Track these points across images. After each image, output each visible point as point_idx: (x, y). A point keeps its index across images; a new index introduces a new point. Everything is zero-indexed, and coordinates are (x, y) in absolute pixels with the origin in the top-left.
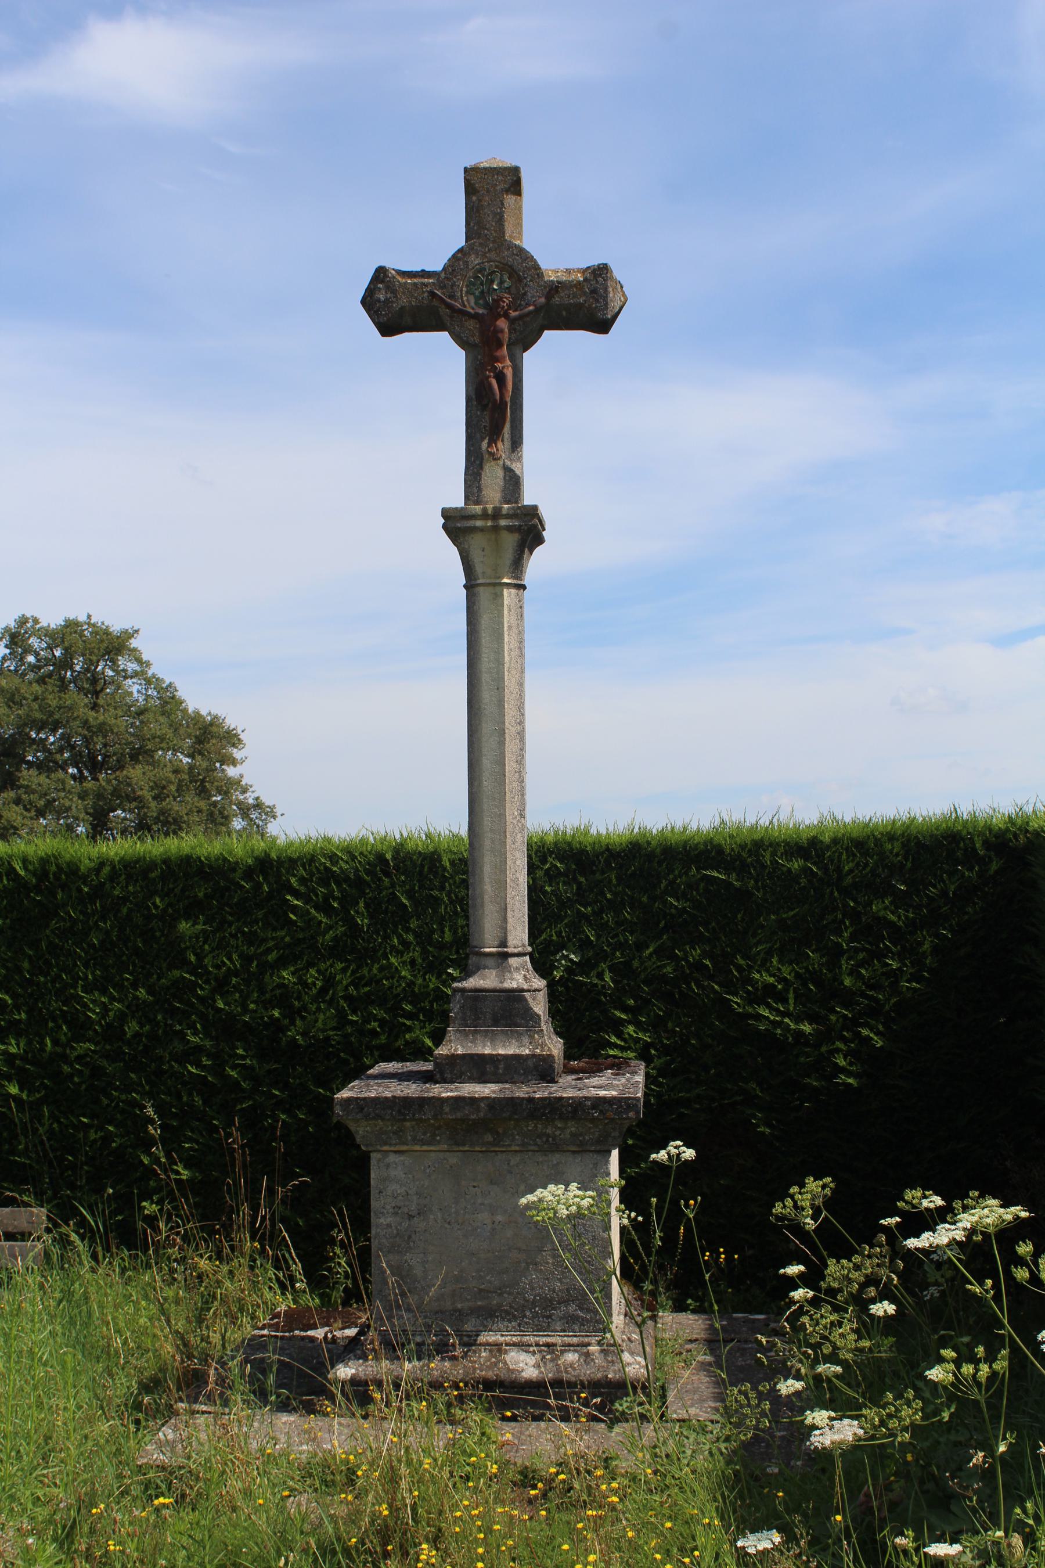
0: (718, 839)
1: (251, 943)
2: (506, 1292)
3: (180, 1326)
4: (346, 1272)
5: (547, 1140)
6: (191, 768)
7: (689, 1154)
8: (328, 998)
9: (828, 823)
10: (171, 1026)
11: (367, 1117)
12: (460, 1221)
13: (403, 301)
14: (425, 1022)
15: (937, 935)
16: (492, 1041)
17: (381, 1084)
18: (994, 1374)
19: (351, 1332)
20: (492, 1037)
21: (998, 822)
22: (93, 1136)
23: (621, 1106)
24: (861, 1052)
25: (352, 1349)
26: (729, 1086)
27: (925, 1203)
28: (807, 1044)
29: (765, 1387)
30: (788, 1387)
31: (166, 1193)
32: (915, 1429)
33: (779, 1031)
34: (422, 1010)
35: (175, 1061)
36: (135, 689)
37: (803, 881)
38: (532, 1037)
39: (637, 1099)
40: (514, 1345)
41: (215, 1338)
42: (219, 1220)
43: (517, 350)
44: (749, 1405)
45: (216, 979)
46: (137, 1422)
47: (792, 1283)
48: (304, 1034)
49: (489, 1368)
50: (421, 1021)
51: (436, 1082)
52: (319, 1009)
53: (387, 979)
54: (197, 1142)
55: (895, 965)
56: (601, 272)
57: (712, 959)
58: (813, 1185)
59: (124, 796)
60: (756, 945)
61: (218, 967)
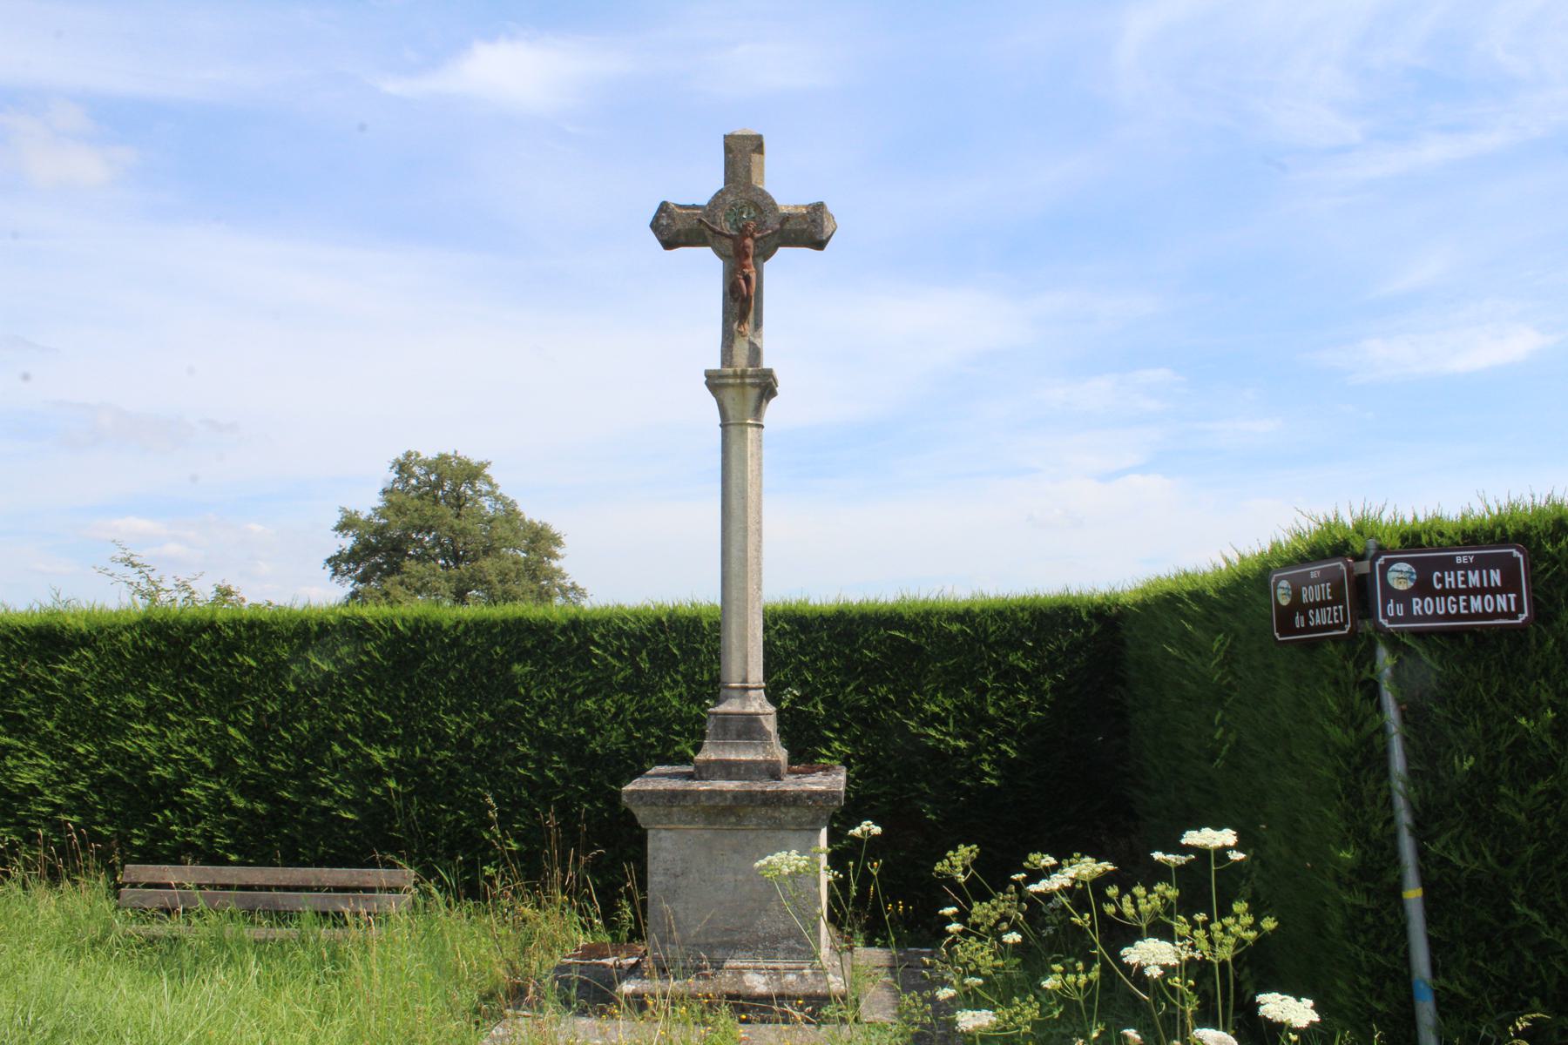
0: (900, 609)
1: (564, 681)
3: (510, 955)
6: (526, 560)
7: (877, 830)
9: (978, 598)
11: (645, 804)
13: (680, 226)
15: (1055, 678)
17: (657, 780)
18: (1089, 983)
19: (633, 960)
20: (735, 747)
21: (1097, 598)
22: (449, 818)
24: (1001, 761)
25: (634, 971)
27: (1043, 863)
28: (962, 755)
29: (927, 994)
30: (944, 993)
32: (1035, 1024)
36: (487, 504)
37: (960, 639)
41: (535, 964)
43: (760, 260)
46: (477, 1023)
47: (947, 920)
48: (602, 746)
55: (1025, 699)
56: (818, 208)
57: (895, 693)
59: (478, 580)
61: (540, 697)
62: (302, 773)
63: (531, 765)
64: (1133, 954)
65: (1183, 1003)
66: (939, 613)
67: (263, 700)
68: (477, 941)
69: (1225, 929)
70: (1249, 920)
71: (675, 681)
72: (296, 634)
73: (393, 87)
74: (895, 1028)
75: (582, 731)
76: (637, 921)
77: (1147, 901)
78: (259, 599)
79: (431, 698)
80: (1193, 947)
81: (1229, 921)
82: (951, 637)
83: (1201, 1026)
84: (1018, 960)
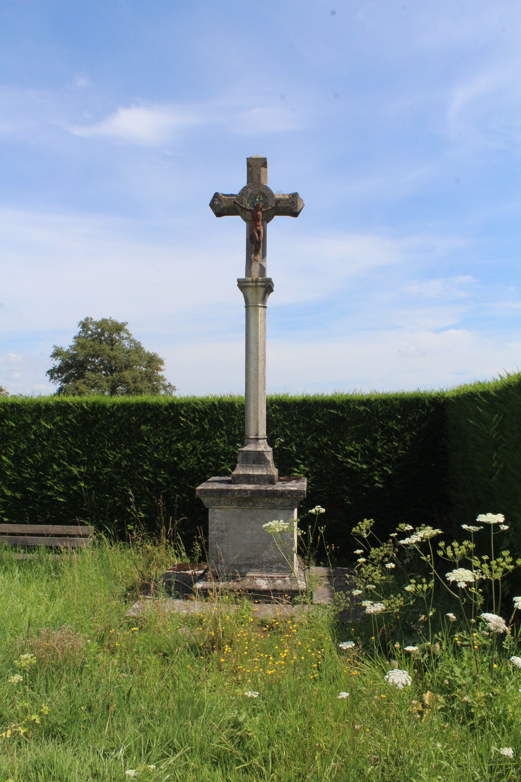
0: (334, 399)
1: (167, 434)
3: (141, 568)
6: (146, 372)
7: (323, 510)
11: (207, 496)
13: (224, 205)
15: (412, 434)
18: (429, 589)
19: (201, 572)
20: (253, 468)
21: (434, 394)
22: (110, 501)
24: (384, 475)
25: (202, 577)
26: (337, 487)
27: (406, 528)
28: (365, 472)
29: (348, 592)
30: (356, 592)
31: (136, 522)
32: (401, 608)
33: (355, 468)
34: (228, 458)
36: (126, 344)
37: (364, 414)
38: (267, 468)
40: (259, 577)
43: (265, 222)
44: (342, 599)
46: (126, 602)
47: (358, 556)
48: (186, 466)
49: (250, 585)
51: (232, 484)
54: (147, 504)
55: (396, 444)
57: (331, 441)
58: (366, 522)
59: (122, 382)
61: (155, 442)
62: (38, 479)
63: (150, 476)
64: (453, 576)
65: (476, 600)
66: (354, 401)
67: (19, 443)
68: (125, 562)
69: (498, 564)
70: (510, 560)
71: (221, 434)
72: (34, 410)
73: (78, 132)
74: (330, 607)
75: (176, 459)
76: (203, 553)
77: (459, 549)
78: (16, 393)
79: (101, 442)
80: (482, 573)
81: (500, 560)
82: (360, 413)
83: (485, 612)
84: (393, 576)
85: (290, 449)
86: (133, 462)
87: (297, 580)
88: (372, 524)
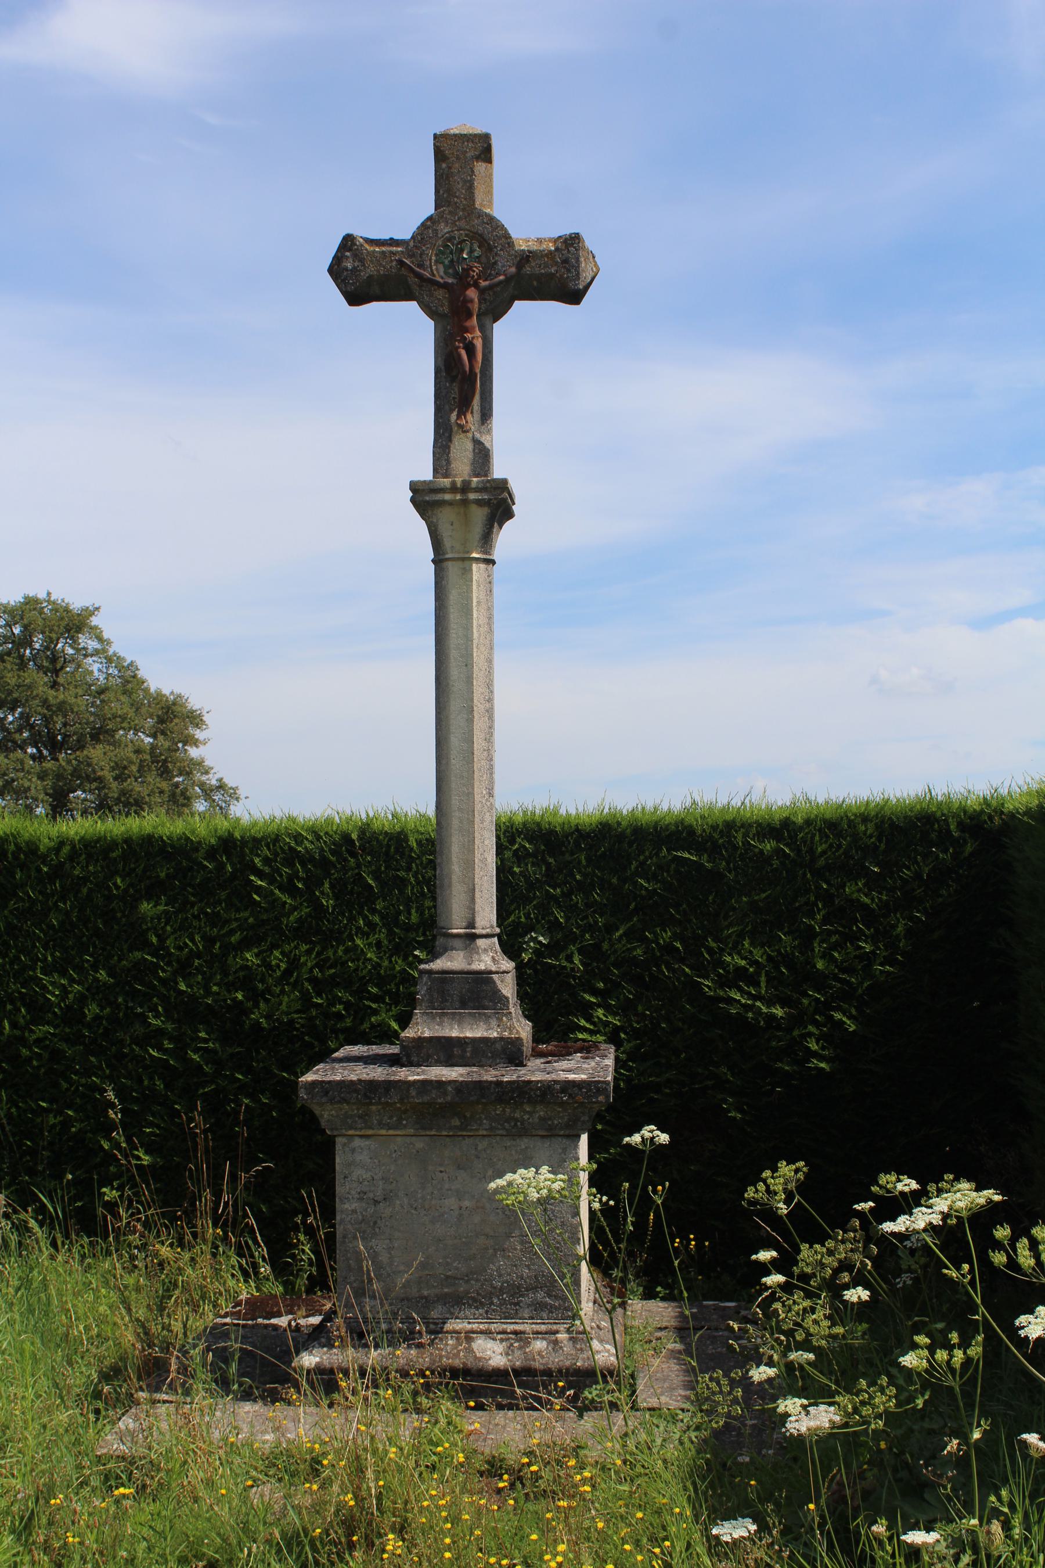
0: (690, 820)
1: (213, 925)
2: (472, 1279)
3: (141, 1313)
4: (310, 1259)
5: (516, 1124)
6: (153, 747)
7: (664, 1138)
8: (292, 980)
9: (803, 805)
10: (132, 1008)
11: (332, 1101)
12: (427, 1207)
13: (371, 270)
14: (390, 1005)
15: (912, 918)
16: (460, 1024)
17: (347, 1067)
18: (968, 1362)
19: (315, 1320)
20: (460, 1020)
21: (973, 804)
22: (52, 1121)
23: (591, 1090)
24: (834, 1035)
25: (318, 1336)
26: (700, 1070)
27: (900, 1187)
28: (779, 1028)
29: (737, 1374)
30: (761, 1373)
31: (126, 1179)
34: (389, 992)
35: (136, 1045)
36: (95, 667)
37: (776, 863)
38: (500, 1020)
39: (607, 1083)
40: (482, 1332)
41: (177, 1326)
42: (180, 1206)
43: (487, 321)
45: (178, 961)
46: (97, 1412)
47: (764, 1269)
48: (268, 1017)
50: (387, 1004)
51: (402, 1066)
52: (283, 991)
53: (353, 961)
54: (158, 1127)
56: (572, 242)
58: (785, 1169)
59: (85, 776)
60: (728, 928)
63: (168, 1045)
75: (240, 996)
85: (565, 963)
86: (118, 1006)
87: (589, 1340)
88: (801, 1176)
